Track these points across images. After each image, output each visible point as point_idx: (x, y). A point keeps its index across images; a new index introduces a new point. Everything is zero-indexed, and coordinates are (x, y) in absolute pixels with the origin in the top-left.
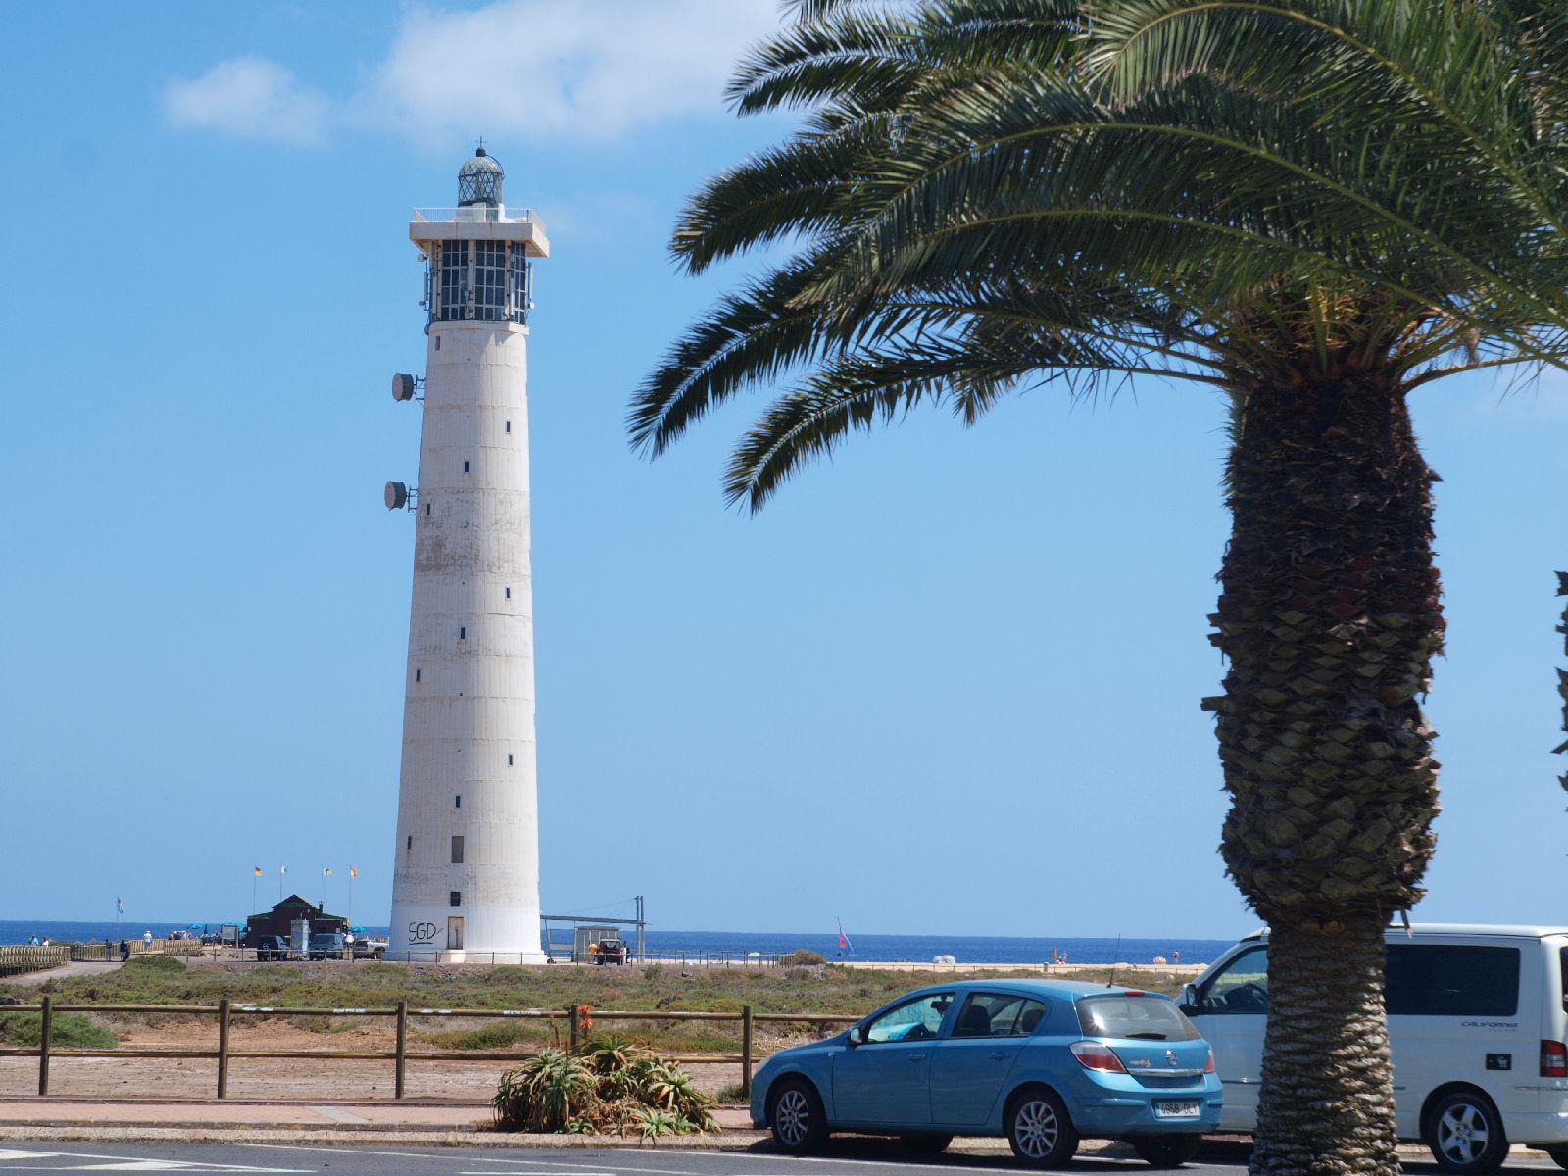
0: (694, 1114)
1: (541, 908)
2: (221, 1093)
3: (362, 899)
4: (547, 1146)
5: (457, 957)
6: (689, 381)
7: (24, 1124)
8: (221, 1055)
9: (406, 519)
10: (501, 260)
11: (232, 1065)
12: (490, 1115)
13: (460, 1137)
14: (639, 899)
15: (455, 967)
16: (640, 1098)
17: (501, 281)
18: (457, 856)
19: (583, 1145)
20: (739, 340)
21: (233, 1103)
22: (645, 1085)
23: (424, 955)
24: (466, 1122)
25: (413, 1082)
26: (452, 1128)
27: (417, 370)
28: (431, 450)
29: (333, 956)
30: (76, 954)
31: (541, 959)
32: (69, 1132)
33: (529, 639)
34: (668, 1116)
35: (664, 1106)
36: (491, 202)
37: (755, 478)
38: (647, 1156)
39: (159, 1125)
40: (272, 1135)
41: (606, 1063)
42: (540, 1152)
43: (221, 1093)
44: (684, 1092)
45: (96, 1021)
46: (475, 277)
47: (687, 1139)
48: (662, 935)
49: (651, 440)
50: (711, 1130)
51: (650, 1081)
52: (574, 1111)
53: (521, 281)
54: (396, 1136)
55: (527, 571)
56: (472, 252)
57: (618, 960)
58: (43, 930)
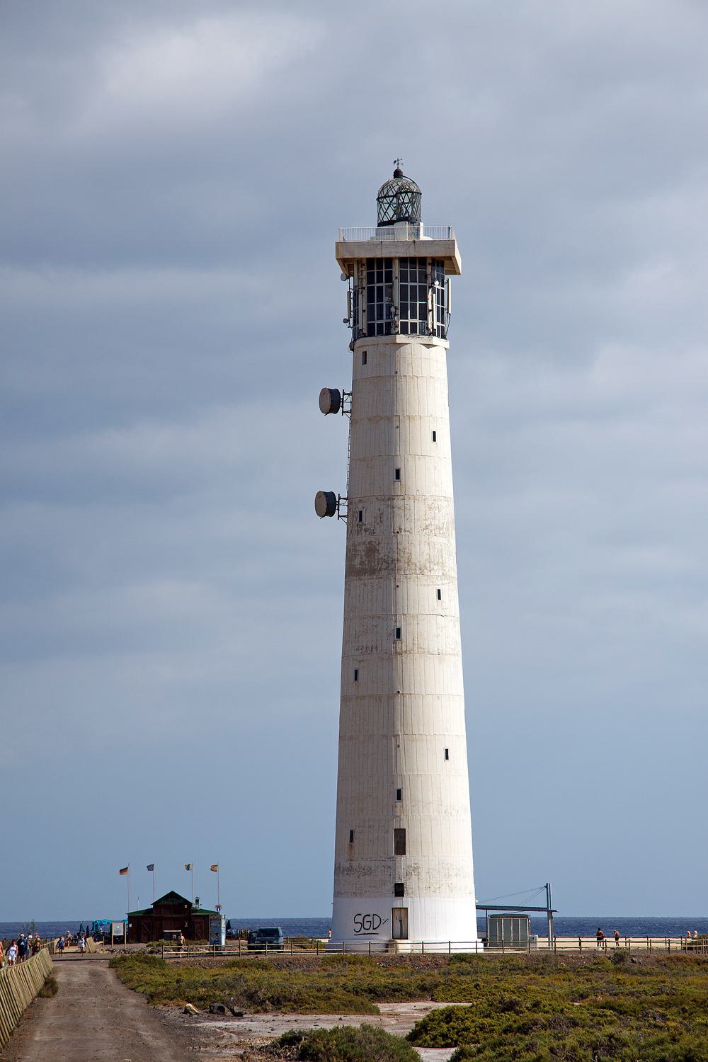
5: (404, 947)
9: (336, 527)
36: (411, 220)
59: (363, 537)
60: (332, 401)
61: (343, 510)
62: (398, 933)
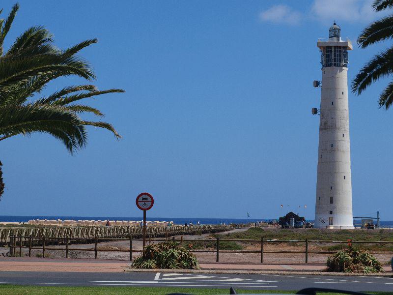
0: (377, 267)
1: (353, 215)
2: (217, 261)
3: (308, 213)
4: (339, 275)
5: (332, 227)
6: (367, 77)
7: (208, 269)
8: (262, 252)
9: (317, 117)
10: (340, 51)
11: (265, 255)
12: (324, 267)
13: (317, 273)
14: (378, 213)
15: (332, 230)
16: (363, 263)
17: (340, 56)
18: (332, 201)
19: (349, 275)
20: (379, 67)
21: (265, 264)
22: (365, 260)
23: (323, 226)
24: (320, 269)
25: (266, 258)
26: (316, 271)
27: (320, 79)
28: (323, 99)
29: (301, 227)
30: (237, 227)
31: (354, 228)
32: (219, 271)
33: (349, 147)
34: (371, 268)
35: (370, 265)
36: (338, 36)
37: (386, 101)
38: (364, 278)
39: (240, 270)
40: (269, 272)
41: (354, 254)
42: (337, 277)
43: (217, 261)
44: (375, 262)
45: (238, 244)
46: (333, 56)
47: (375, 274)
48: (384, 222)
49: (357, 91)
50: (382, 272)
51: (366, 259)
52: (346, 267)
53: (346, 56)
54: (301, 273)
55: (348, 130)
56: (333, 50)
57: (373, 228)
58: (224, 221)
59: (323, 120)
60: (315, 111)
61: (319, 113)
62: (330, 224)
